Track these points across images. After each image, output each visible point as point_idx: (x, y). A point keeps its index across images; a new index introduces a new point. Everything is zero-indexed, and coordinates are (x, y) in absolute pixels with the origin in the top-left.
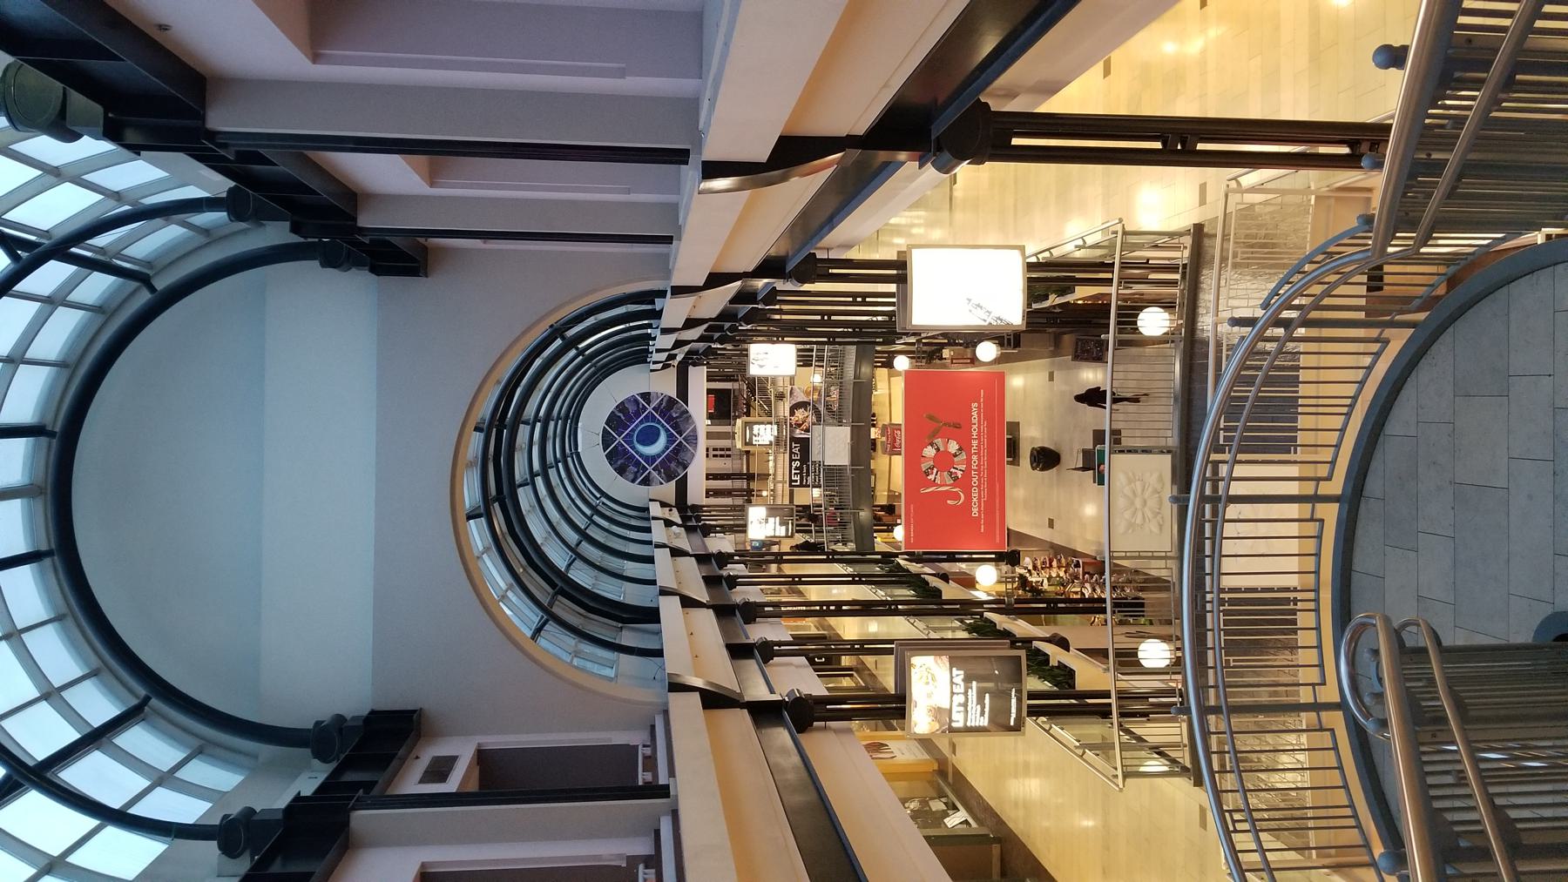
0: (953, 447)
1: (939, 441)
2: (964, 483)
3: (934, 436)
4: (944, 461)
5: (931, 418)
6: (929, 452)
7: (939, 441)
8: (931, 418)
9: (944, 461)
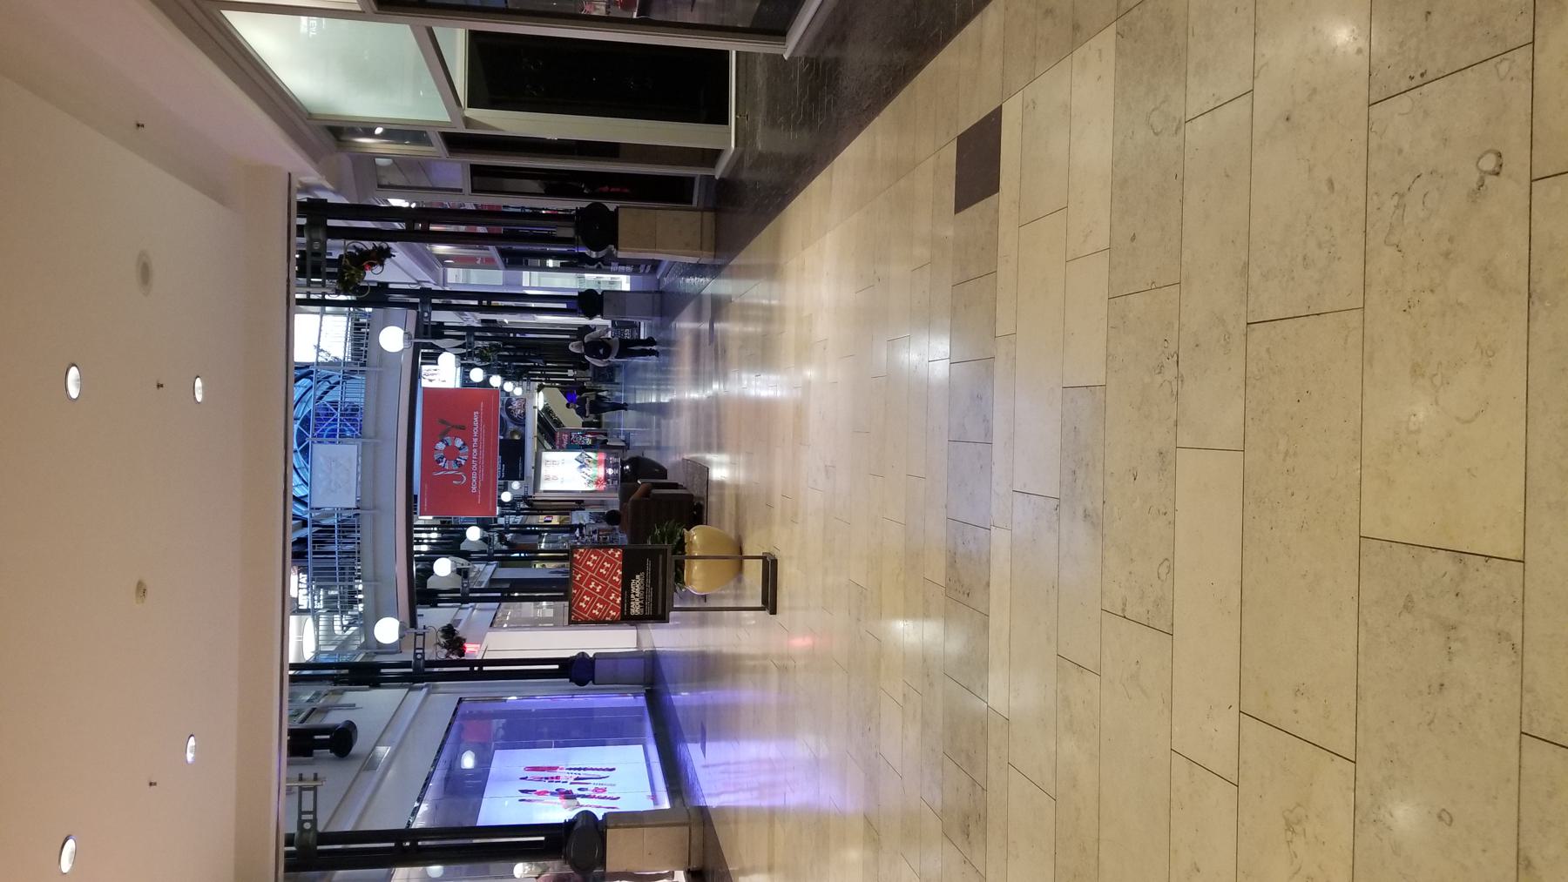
0: (459, 443)
1: (448, 439)
2: (467, 469)
3: (445, 434)
4: (451, 453)
5: (443, 422)
6: (441, 446)
7: (448, 439)
8: (443, 422)
9: (451, 453)
